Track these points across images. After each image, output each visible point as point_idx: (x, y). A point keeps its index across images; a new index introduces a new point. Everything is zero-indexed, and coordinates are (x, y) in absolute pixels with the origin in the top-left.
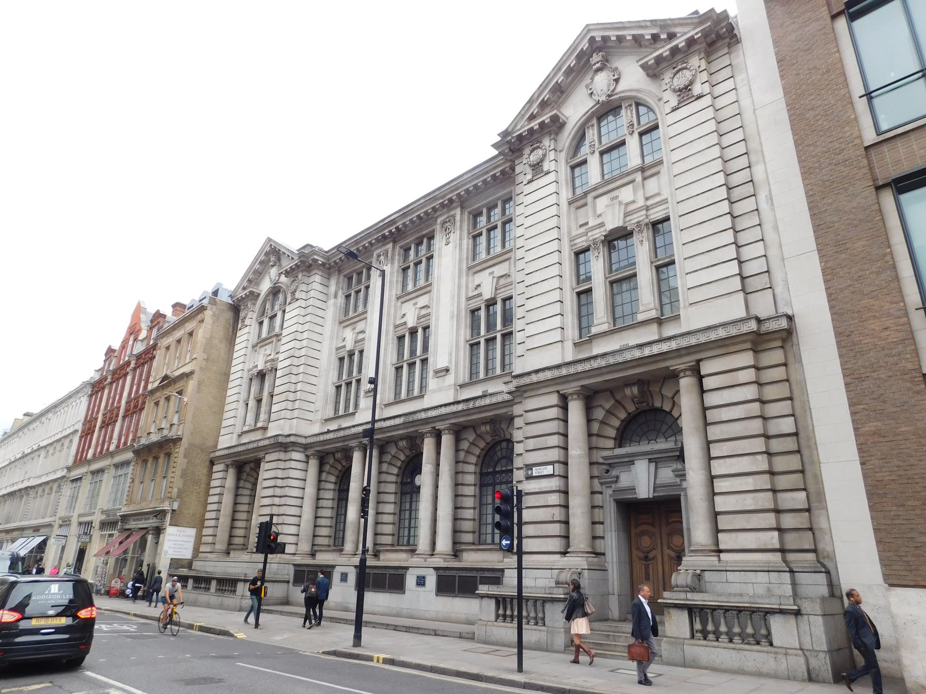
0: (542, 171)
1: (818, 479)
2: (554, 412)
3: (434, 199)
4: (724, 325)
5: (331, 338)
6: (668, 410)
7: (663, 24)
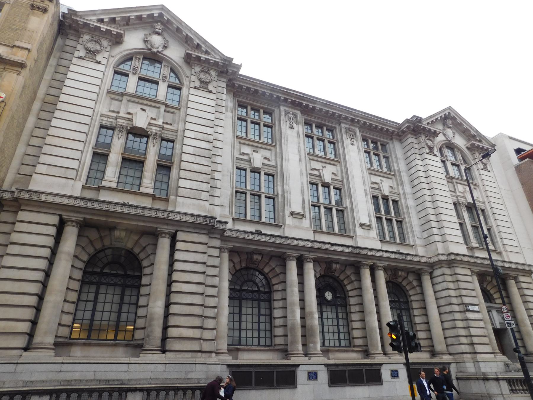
2: (52, 231)
3: (350, 113)
7: (480, 135)
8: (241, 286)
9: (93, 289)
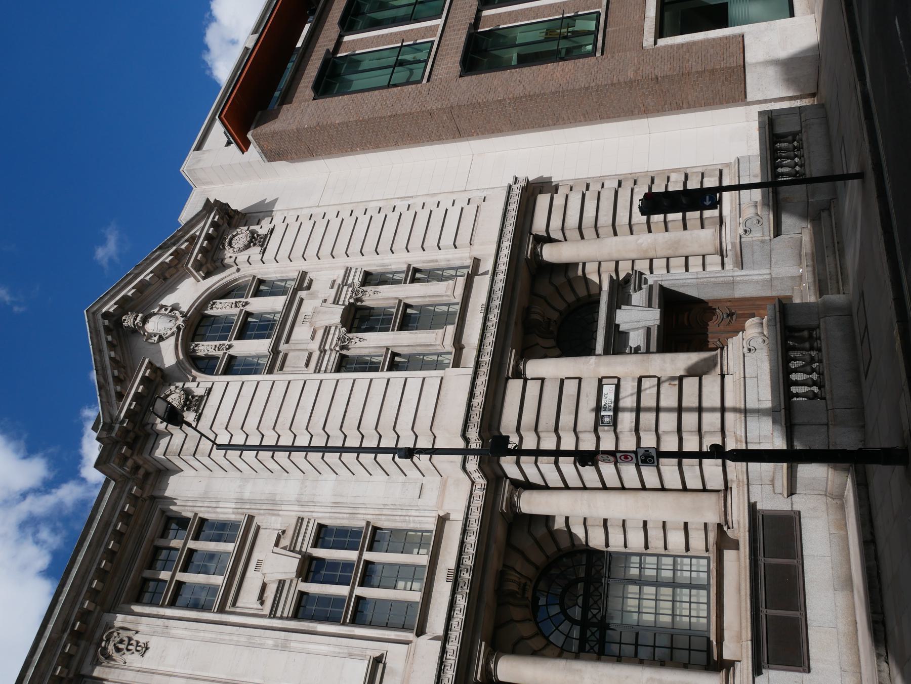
8: (574, 622)
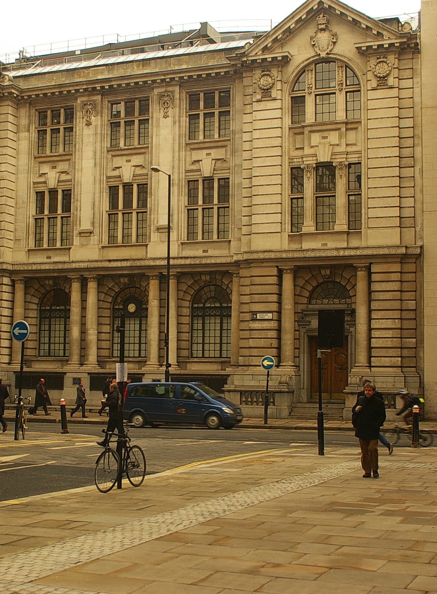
0: (271, 96)
1: (422, 334)
2: (274, 280)
4: (388, 247)
5: (29, 172)
6: (348, 289)
9: (200, 319)
